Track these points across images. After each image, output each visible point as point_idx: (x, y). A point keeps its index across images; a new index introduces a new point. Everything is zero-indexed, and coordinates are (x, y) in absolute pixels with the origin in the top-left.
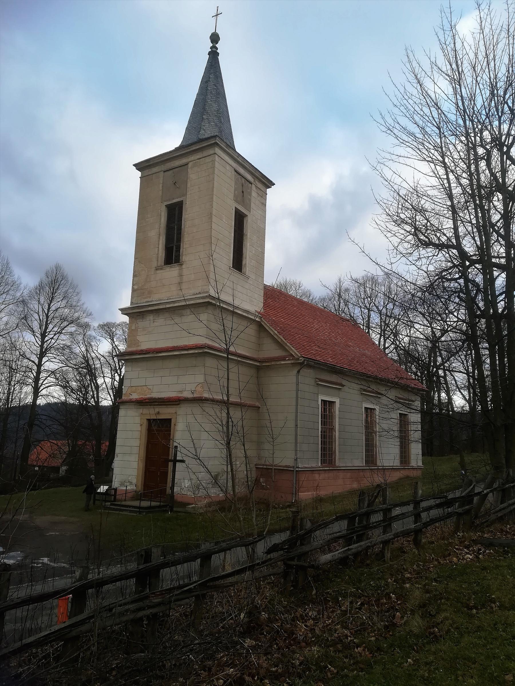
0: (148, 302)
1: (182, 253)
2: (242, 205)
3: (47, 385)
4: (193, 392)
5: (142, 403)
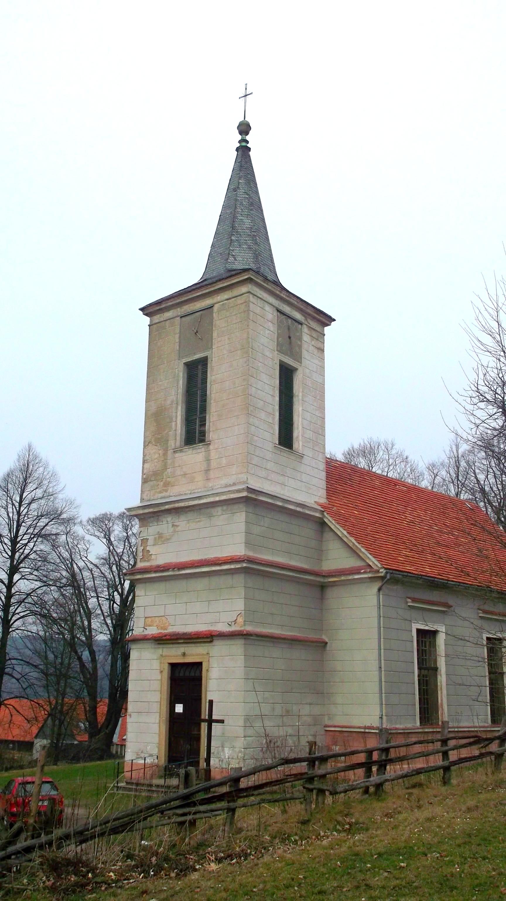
1: (209, 429)
2: (289, 356)
3: (22, 614)
4: (230, 623)
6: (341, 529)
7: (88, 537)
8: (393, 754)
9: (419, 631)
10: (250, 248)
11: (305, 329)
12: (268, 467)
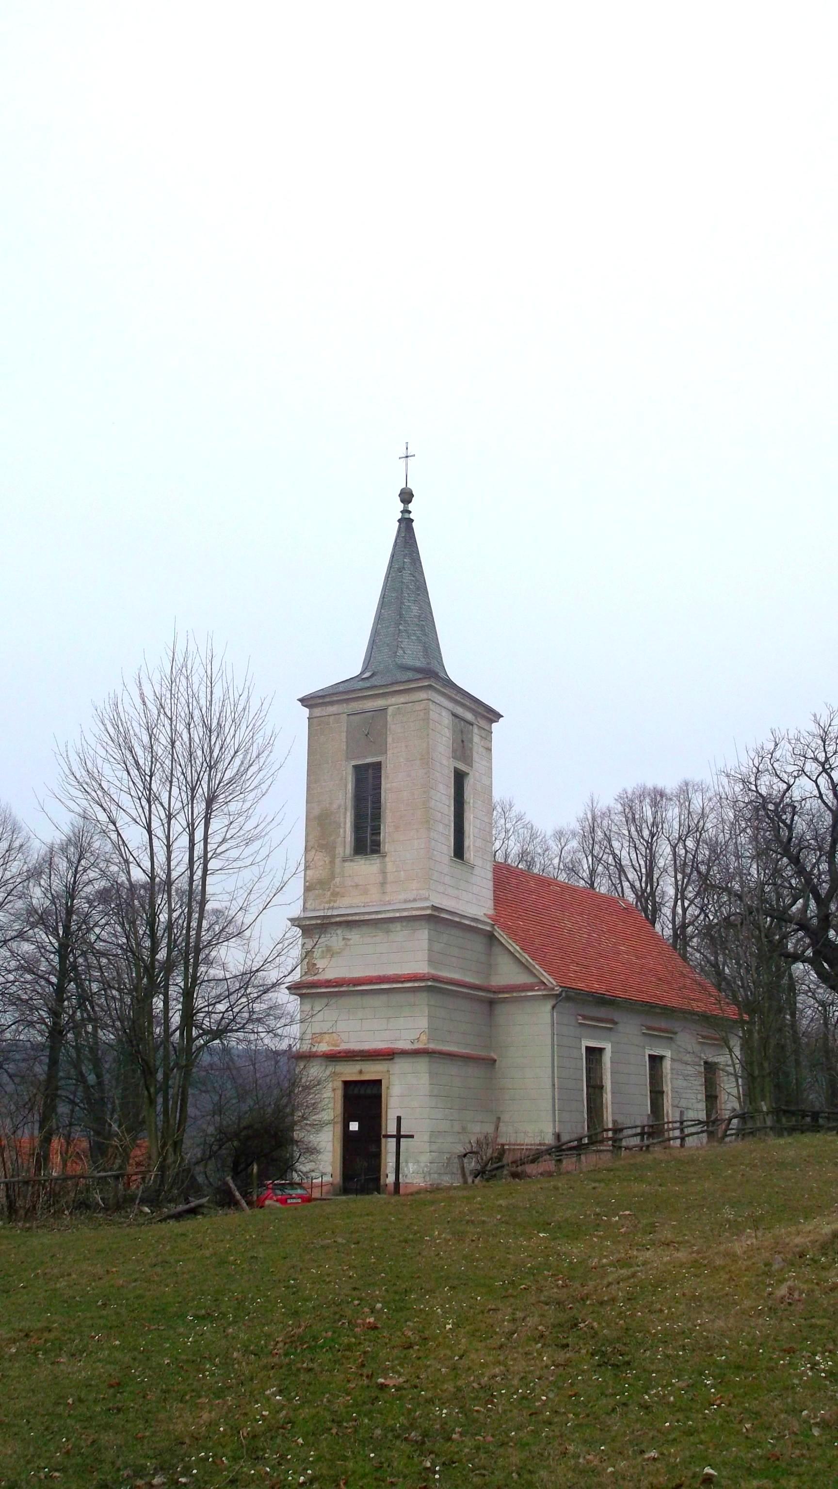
1: (384, 840)
6: (514, 945)
9: (587, 1048)
11: (476, 730)
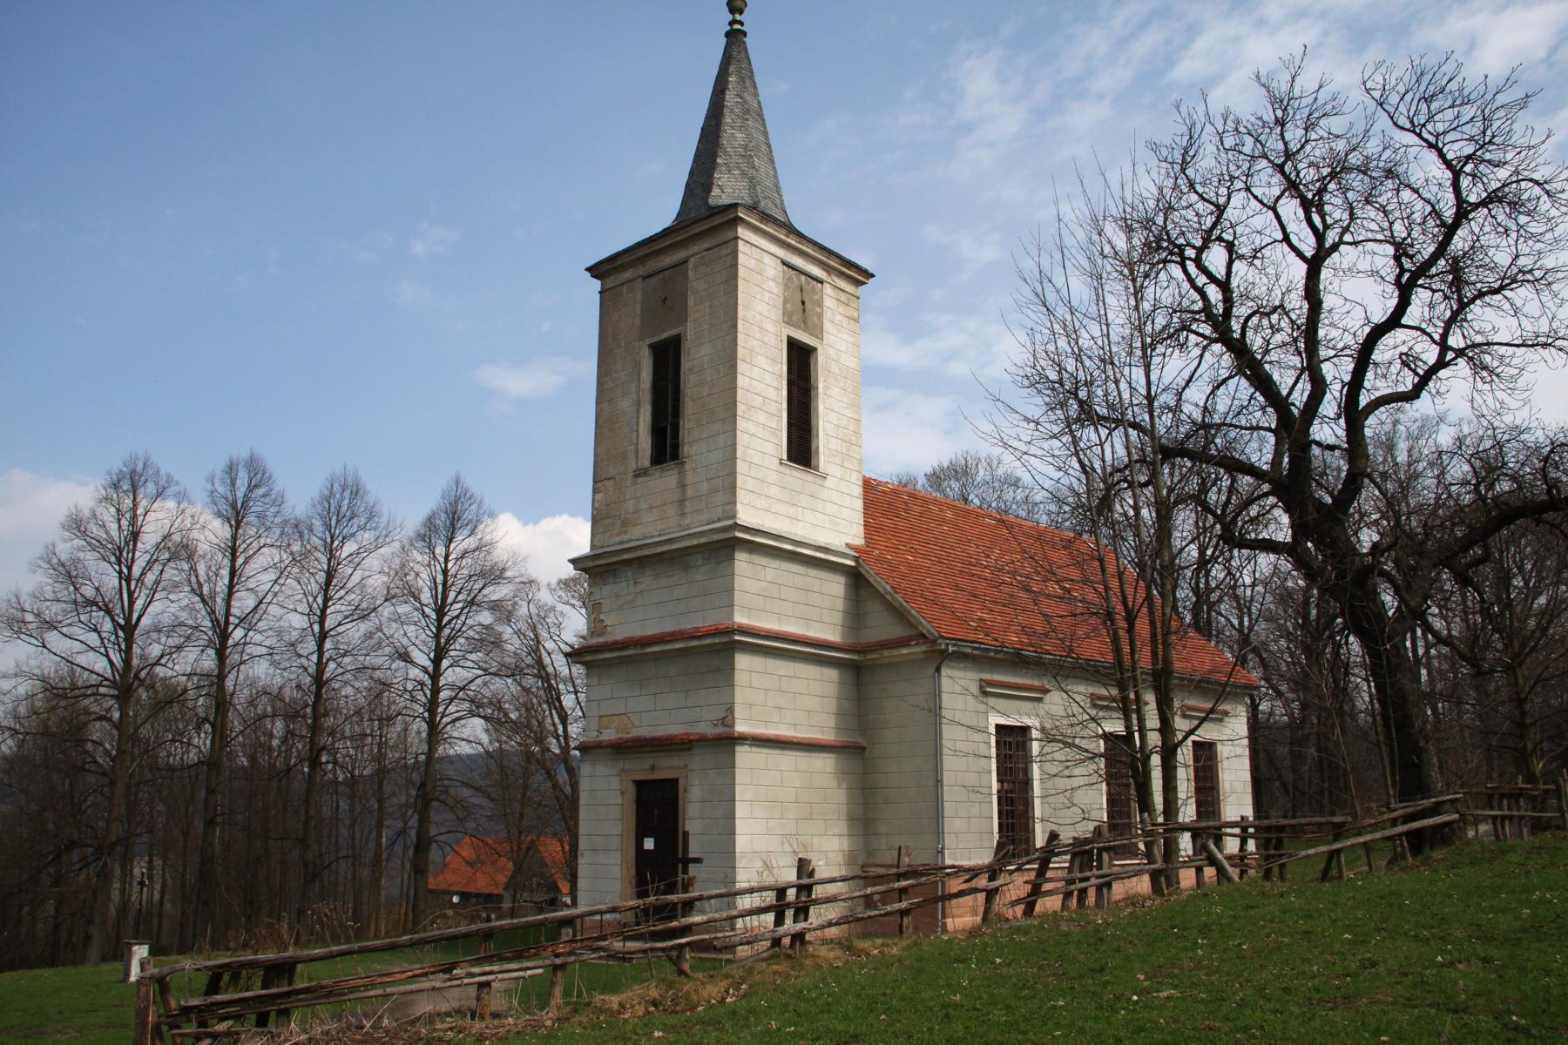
0: (622, 543)
5: (623, 749)
7: (560, 607)
8: (818, 892)
9: (998, 727)
10: (744, 174)
11: (828, 289)
12: (771, 494)
